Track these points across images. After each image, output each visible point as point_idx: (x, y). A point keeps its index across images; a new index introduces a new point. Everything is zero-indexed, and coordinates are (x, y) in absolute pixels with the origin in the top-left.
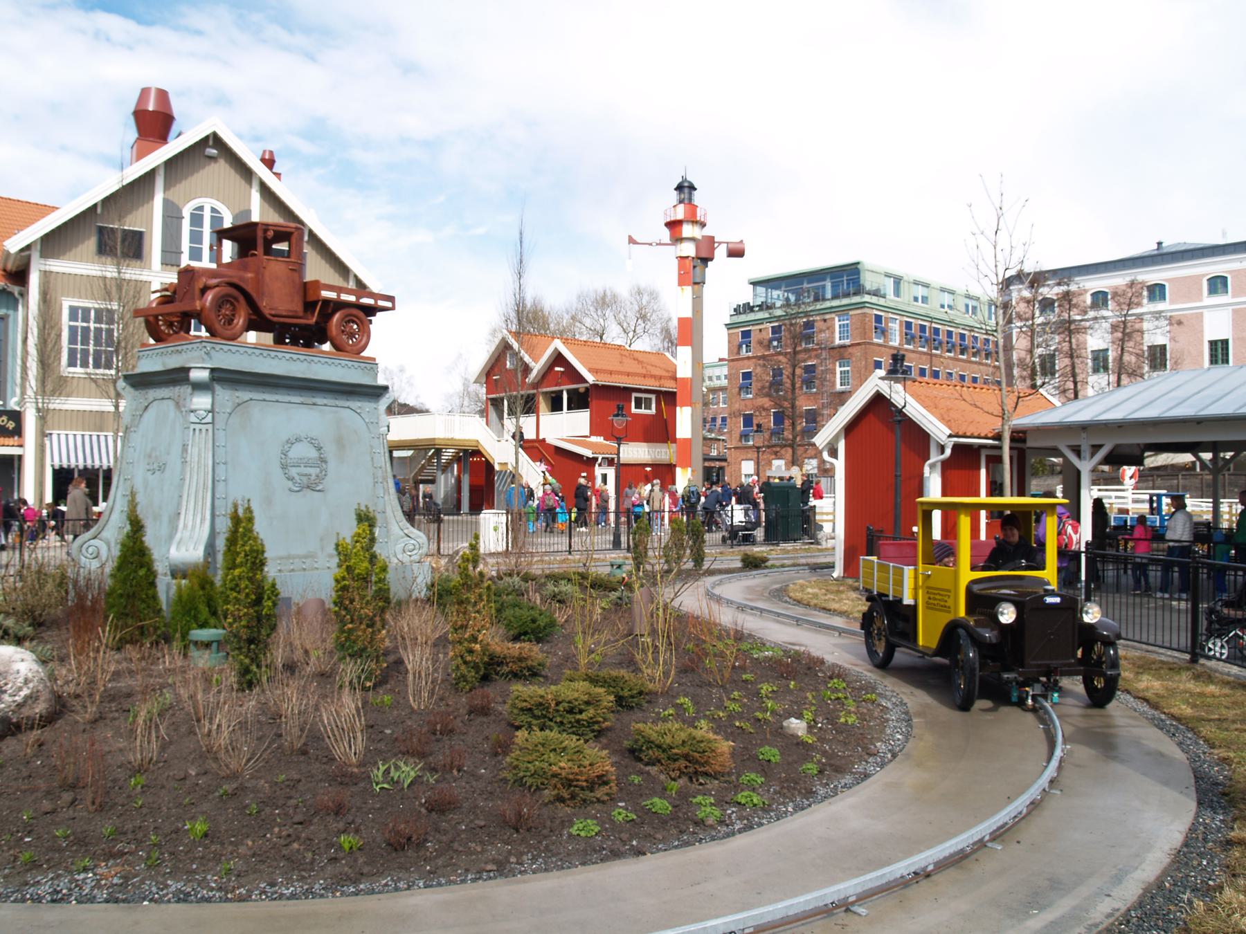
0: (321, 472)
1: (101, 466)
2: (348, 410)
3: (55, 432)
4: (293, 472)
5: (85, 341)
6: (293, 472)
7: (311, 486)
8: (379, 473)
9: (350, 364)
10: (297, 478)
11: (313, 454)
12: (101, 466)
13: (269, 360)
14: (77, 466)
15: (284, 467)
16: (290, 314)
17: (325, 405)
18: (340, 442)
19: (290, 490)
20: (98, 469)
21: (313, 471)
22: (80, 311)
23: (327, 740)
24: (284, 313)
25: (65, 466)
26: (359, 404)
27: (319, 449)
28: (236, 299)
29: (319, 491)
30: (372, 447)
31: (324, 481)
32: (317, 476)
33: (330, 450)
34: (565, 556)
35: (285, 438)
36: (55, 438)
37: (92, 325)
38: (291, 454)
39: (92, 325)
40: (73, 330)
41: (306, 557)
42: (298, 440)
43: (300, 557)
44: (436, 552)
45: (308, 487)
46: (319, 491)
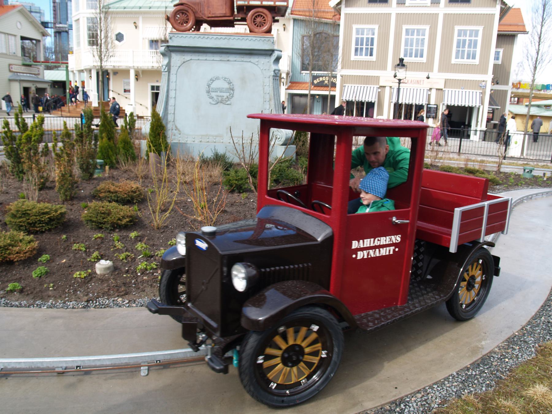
0: (230, 95)
1: (476, 106)
2: (250, 63)
3: (347, 85)
4: (213, 94)
5: (464, 46)
6: (213, 94)
7: (221, 101)
8: (267, 97)
9: (254, 39)
10: (215, 97)
11: (226, 86)
12: (476, 106)
13: (204, 40)
14: (355, 100)
15: (208, 92)
16: (222, 15)
17: (235, 61)
18: (243, 80)
19: (210, 103)
20: (467, 107)
21: (225, 95)
22: (474, 32)
23: (167, 216)
24: (219, 15)
25: (460, 105)
26: (257, 60)
27: (230, 83)
28: (187, 11)
29: (228, 104)
30: (264, 82)
31: (231, 100)
32: (227, 97)
33: (237, 84)
34: (456, 156)
35: (210, 78)
36: (346, 87)
37: (468, 38)
38: (212, 86)
39: (468, 38)
40: (407, 40)
41: (216, 136)
42: (217, 78)
43: (213, 136)
44: (458, 151)
45: (221, 102)
46: (228, 104)
